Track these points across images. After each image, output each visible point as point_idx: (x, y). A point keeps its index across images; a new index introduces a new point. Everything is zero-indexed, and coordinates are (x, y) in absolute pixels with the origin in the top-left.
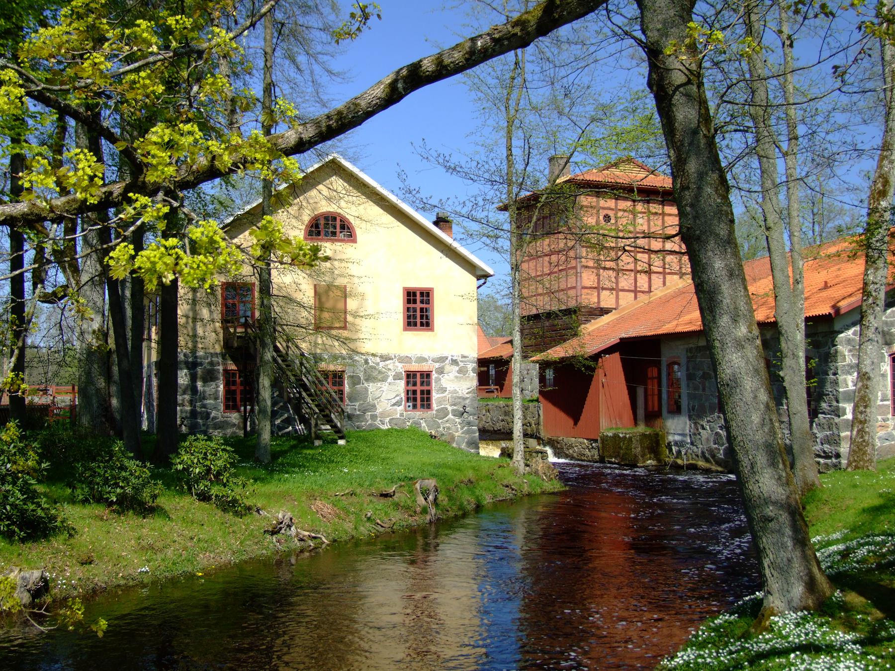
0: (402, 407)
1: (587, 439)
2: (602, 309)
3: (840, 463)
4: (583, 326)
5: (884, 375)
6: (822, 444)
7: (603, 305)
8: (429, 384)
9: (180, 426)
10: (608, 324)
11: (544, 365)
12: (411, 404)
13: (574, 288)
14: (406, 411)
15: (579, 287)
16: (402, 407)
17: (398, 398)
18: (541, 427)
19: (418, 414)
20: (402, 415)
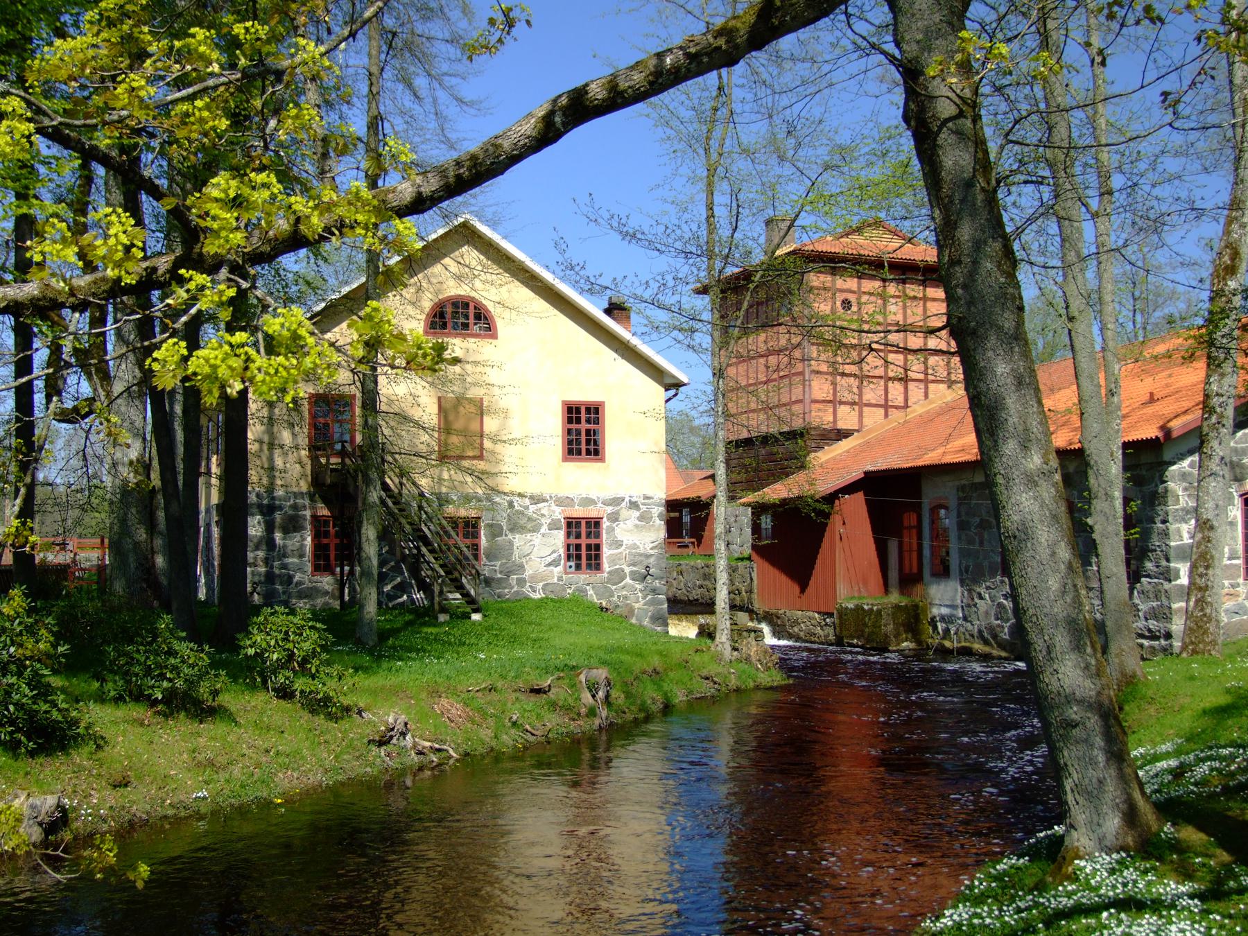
0: (560, 568)
1: (819, 613)
2: (839, 431)
3: (1171, 645)
4: (812, 455)
5: (1232, 524)
6: (1146, 619)
7: (841, 425)
8: (598, 535)
9: (252, 594)
10: (848, 451)
11: (759, 509)
12: (573, 564)
13: (801, 401)
14: (566, 573)
15: (807, 401)
16: (560, 568)
17: (555, 555)
18: (755, 596)
19: (583, 577)
20: (560, 579)
